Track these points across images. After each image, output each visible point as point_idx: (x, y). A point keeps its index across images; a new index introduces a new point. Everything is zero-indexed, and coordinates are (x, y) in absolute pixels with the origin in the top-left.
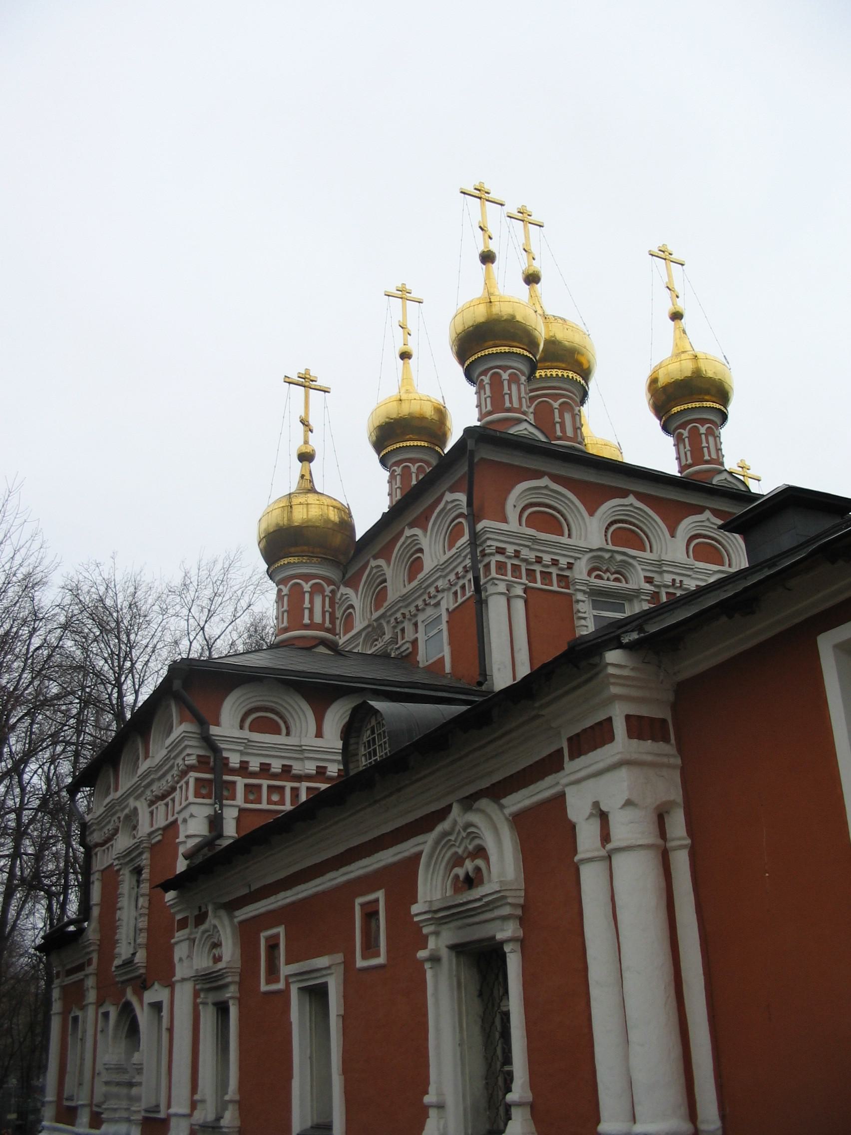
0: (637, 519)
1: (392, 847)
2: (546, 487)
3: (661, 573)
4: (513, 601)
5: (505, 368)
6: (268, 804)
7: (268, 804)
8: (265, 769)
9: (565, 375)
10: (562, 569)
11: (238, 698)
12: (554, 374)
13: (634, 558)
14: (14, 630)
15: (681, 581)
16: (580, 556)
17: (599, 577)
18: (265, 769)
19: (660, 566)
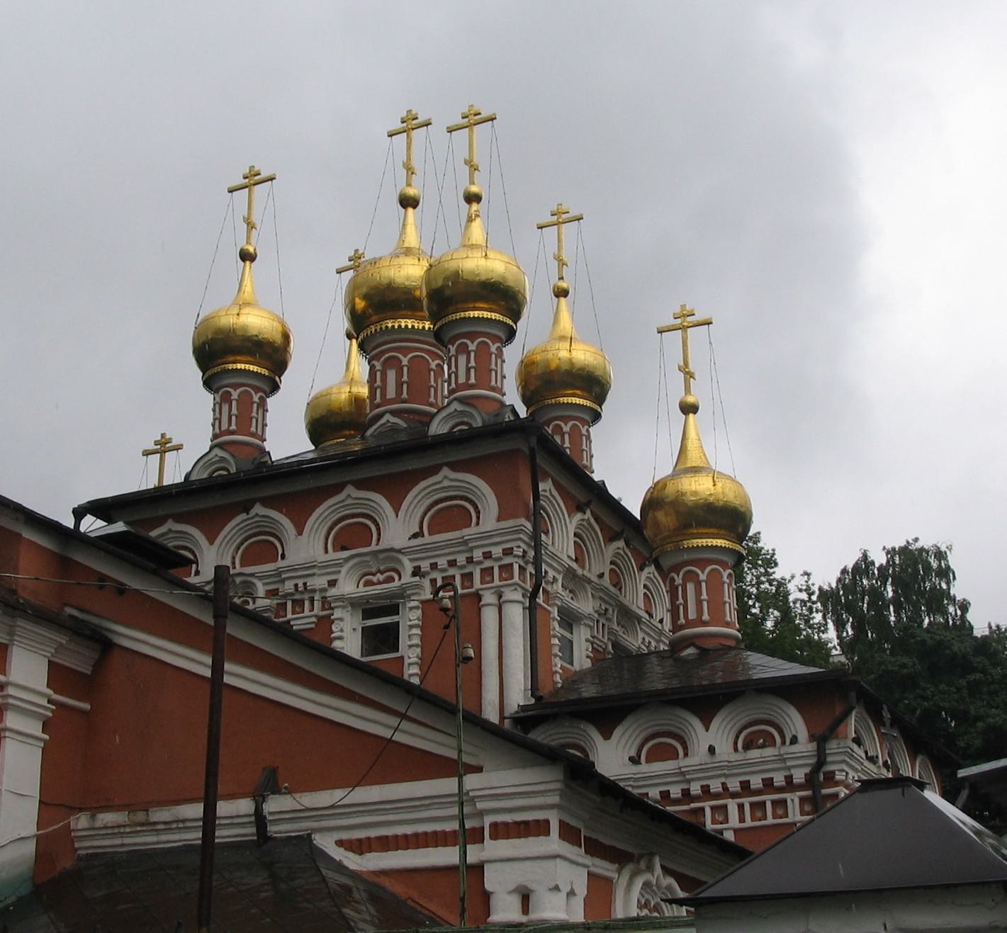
0: (267, 526)
1: (601, 859)
2: (170, 530)
3: (283, 581)
4: (506, 608)
5: (235, 386)
6: (774, 818)
7: (774, 818)
8: (768, 785)
9: (403, 325)
10: (462, 567)
11: (723, 720)
12: (403, 325)
13: (252, 575)
14: (583, 690)
15: (305, 584)
16: (338, 569)
17: (368, 583)
18: (768, 785)
19: (279, 574)
